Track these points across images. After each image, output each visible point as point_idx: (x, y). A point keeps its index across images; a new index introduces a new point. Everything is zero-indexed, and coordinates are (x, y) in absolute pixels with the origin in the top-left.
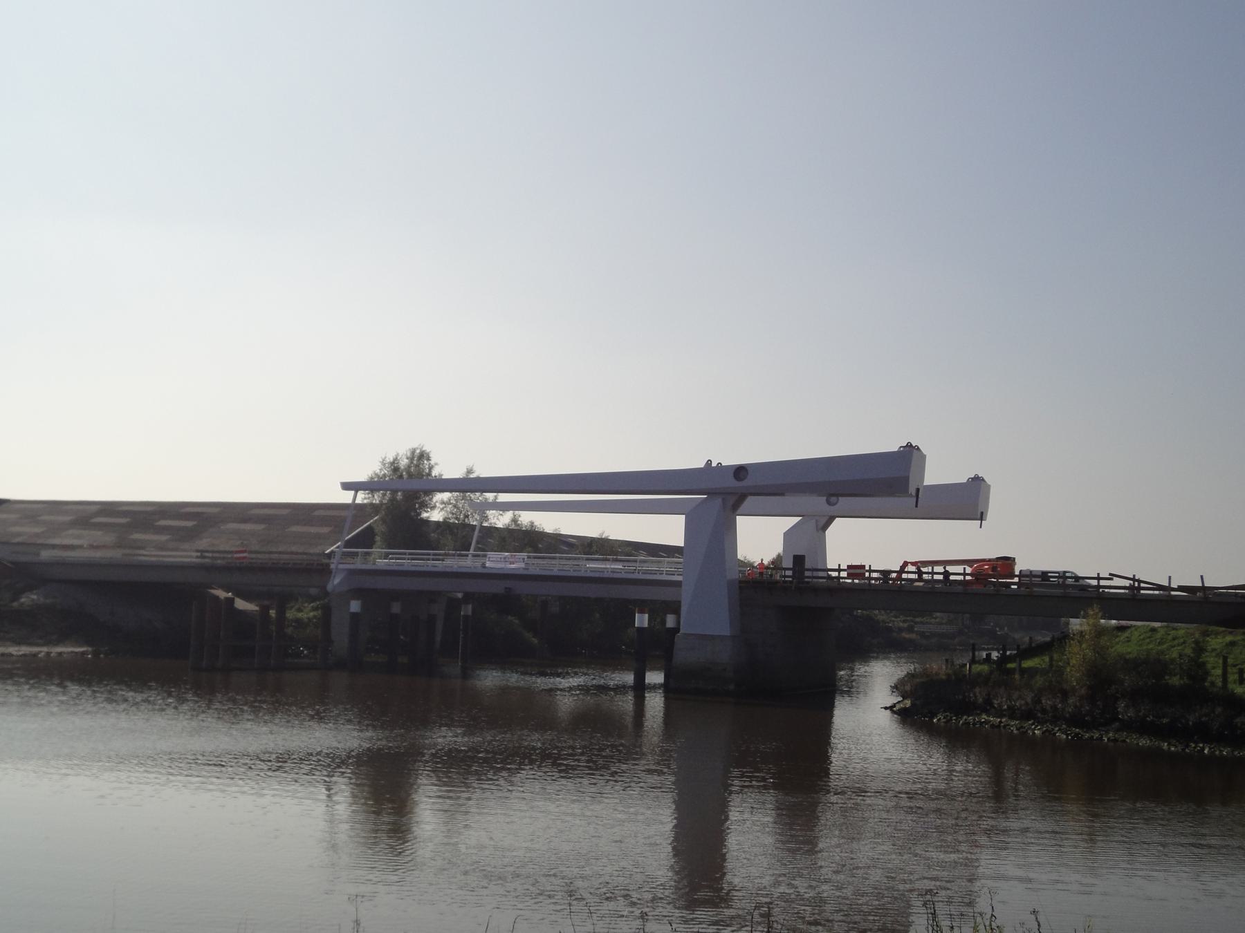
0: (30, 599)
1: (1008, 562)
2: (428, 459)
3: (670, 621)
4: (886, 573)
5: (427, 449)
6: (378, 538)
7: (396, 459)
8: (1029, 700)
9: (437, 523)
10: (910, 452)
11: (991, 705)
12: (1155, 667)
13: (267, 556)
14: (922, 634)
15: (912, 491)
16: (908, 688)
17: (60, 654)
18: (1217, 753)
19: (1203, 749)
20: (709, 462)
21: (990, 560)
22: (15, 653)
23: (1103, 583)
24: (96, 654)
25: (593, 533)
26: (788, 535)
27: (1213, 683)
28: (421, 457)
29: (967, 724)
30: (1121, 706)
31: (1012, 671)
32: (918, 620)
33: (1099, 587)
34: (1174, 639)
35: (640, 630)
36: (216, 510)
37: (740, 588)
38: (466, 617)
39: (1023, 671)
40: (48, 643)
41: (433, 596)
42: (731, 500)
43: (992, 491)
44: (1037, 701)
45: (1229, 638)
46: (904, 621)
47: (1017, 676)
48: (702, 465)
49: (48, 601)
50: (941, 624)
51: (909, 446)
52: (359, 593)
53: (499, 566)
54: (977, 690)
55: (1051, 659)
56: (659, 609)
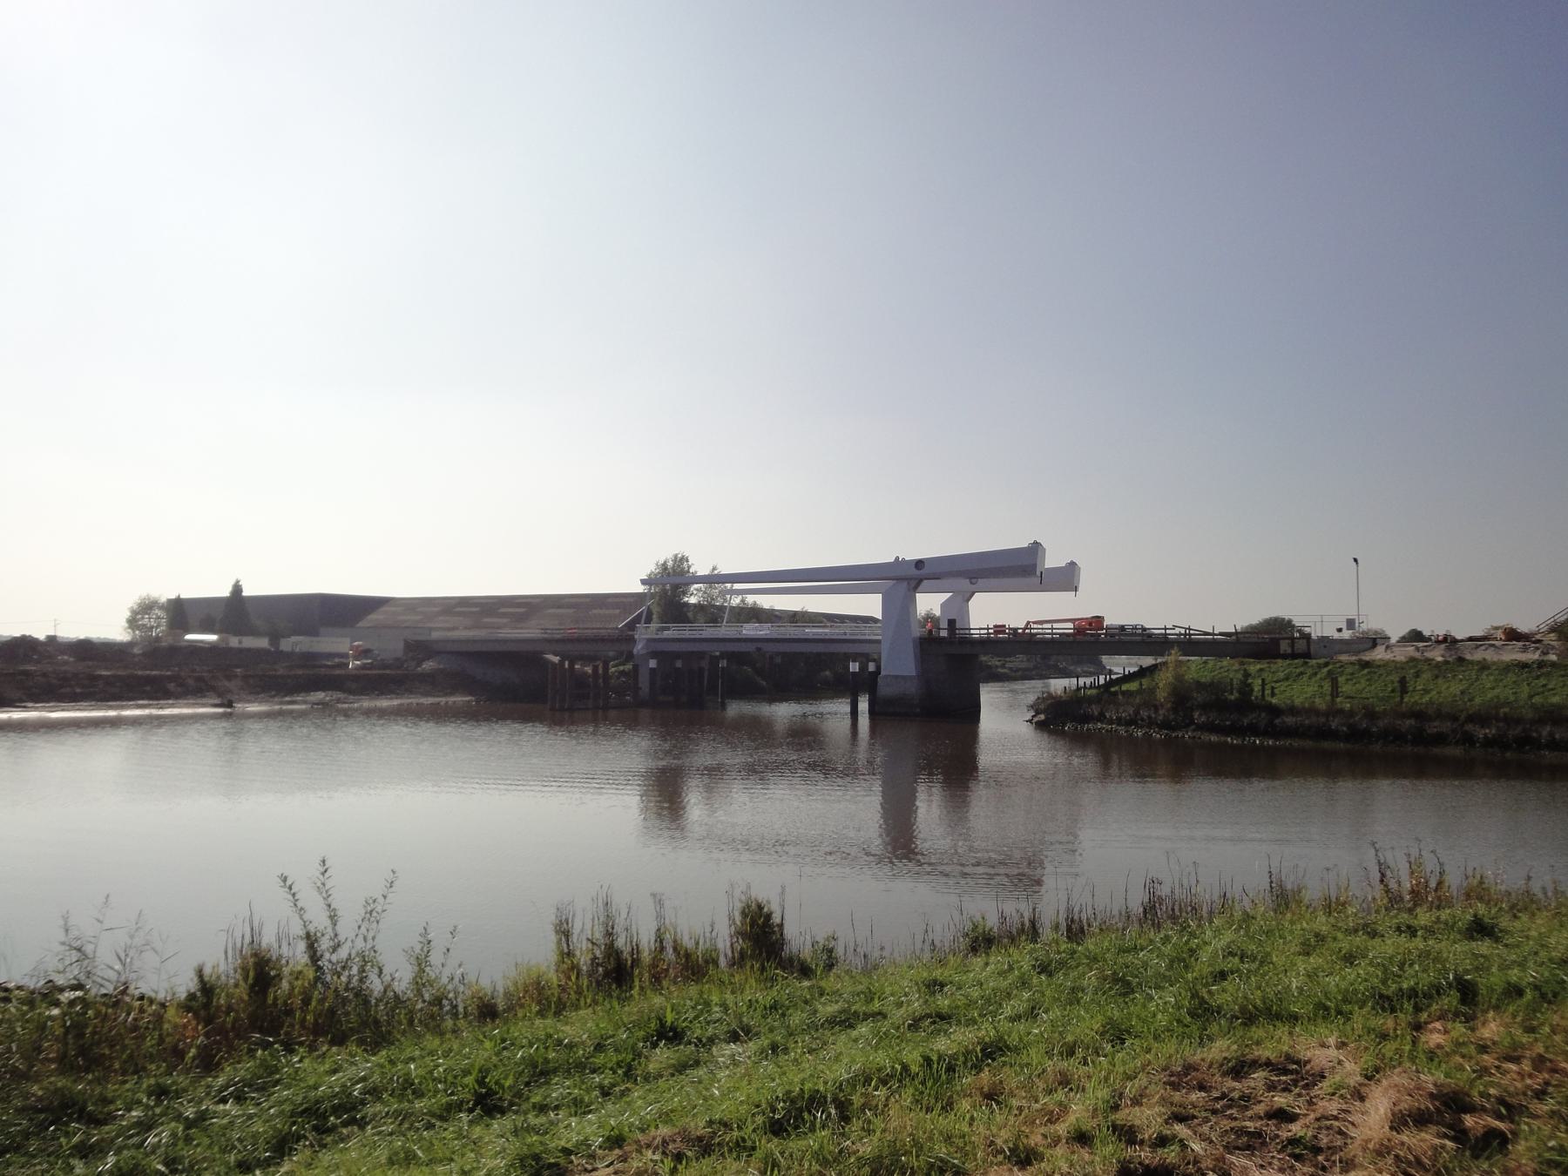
0: (428, 666)
1: (1099, 619)
2: (687, 561)
3: (872, 667)
4: (1015, 630)
6: (654, 616)
7: (665, 562)
8: (1131, 712)
9: (694, 605)
12: (1214, 687)
14: (1011, 669)
15: (1038, 573)
16: (1042, 707)
17: (455, 702)
18: (1266, 743)
19: (1255, 741)
20: (237, 589)
21: (1087, 619)
22: (425, 702)
23: (1168, 631)
25: (797, 608)
26: (943, 606)
28: (681, 560)
29: (1088, 729)
30: (1196, 715)
31: (1115, 693)
32: (1008, 659)
33: (1166, 634)
34: (1221, 668)
35: (854, 673)
36: (538, 600)
37: (921, 644)
38: (723, 668)
39: (1124, 693)
40: (446, 695)
41: (701, 655)
42: (913, 583)
43: (1082, 571)
44: (1137, 713)
45: (1258, 667)
46: (999, 661)
47: (1120, 697)
48: (225, 591)
49: (441, 666)
50: (1022, 661)
51: (1036, 543)
52: (654, 654)
53: (752, 633)
54: (1094, 706)
55: (1141, 685)
56: (864, 658)
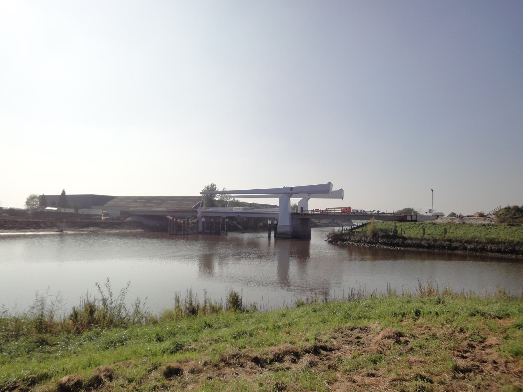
0: (128, 219)
2: (215, 186)
4: (322, 211)
5: (215, 184)
9: (217, 200)
10: (329, 184)
11: (350, 240)
12: (386, 231)
13: (183, 209)
14: (322, 223)
19: (398, 248)
24: (145, 231)
27: (399, 234)
28: (213, 186)
30: (380, 239)
38: (226, 222)
40: (134, 229)
41: (219, 217)
42: (290, 195)
45: (400, 224)
47: (356, 233)
52: (204, 217)
54: (347, 236)
